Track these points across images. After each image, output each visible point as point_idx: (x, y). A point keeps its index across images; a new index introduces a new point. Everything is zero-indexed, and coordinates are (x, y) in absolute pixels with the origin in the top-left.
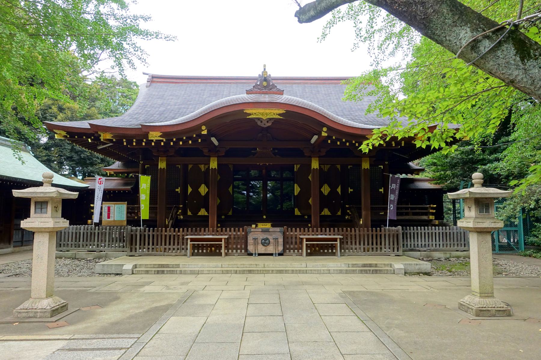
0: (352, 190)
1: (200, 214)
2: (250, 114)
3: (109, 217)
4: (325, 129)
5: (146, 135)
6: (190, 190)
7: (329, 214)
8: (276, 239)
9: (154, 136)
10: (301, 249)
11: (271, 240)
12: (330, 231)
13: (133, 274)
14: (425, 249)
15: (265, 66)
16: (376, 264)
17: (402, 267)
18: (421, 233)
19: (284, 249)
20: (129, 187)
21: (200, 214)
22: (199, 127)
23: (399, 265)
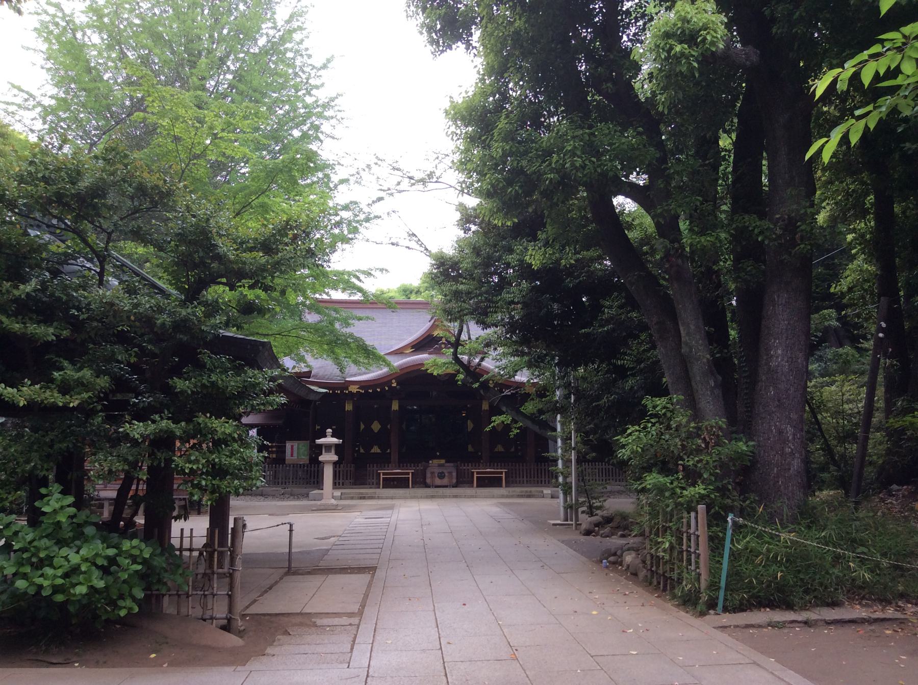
1: (372, 451)
3: (292, 455)
6: (362, 427)
7: (379, 451)
8: (450, 473)
9: (354, 389)
10: (473, 482)
20: (280, 422)
21: (372, 451)
22: (390, 382)
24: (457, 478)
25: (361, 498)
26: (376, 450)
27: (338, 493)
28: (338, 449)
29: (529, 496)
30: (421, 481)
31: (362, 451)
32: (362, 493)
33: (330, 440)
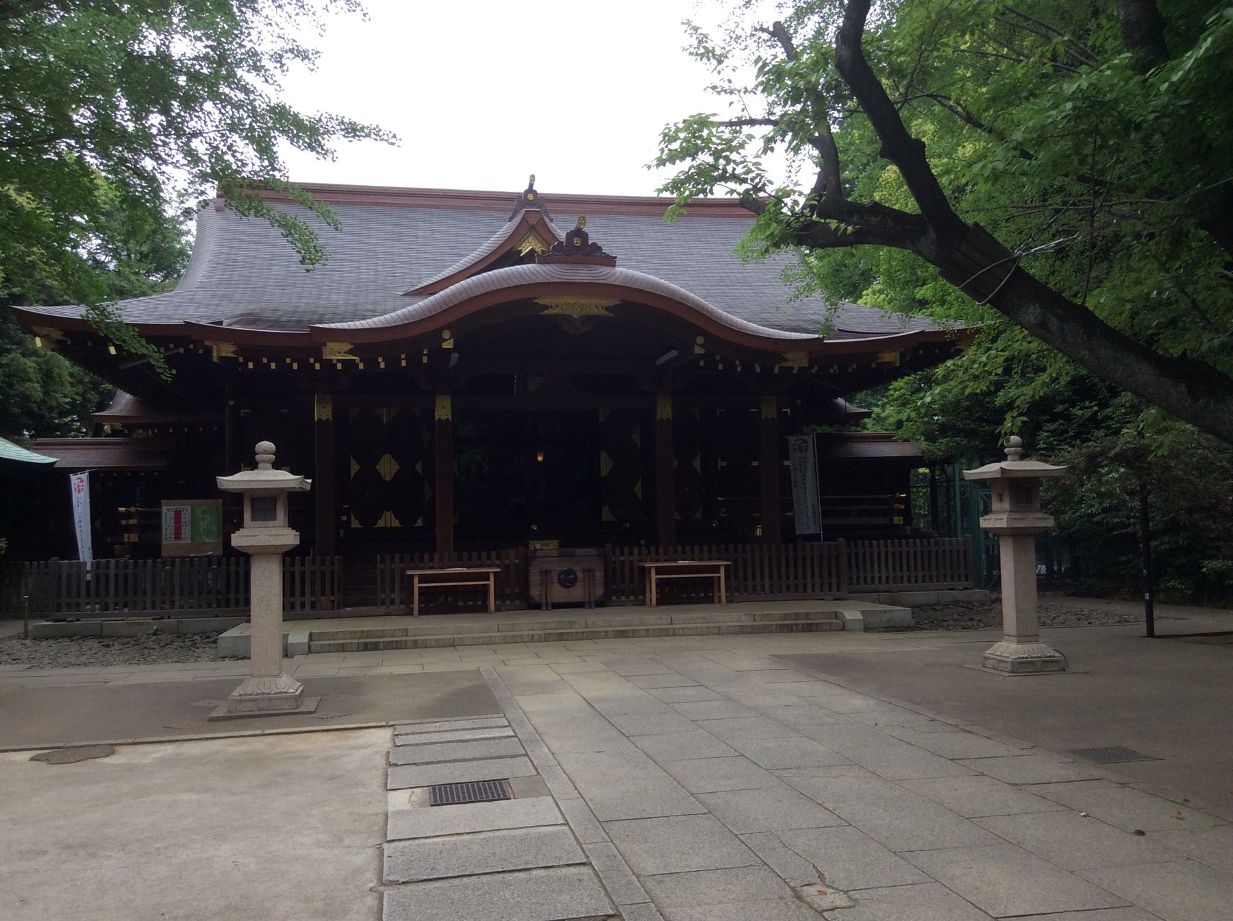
0: (724, 464)
2: (546, 307)
3: (178, 536)
4: (700, 340)
5: (317, 352)
6: (355, 467)
8: (589, 572)
9: (336, 353)
11: (580, 575)
12: (701, 552)
13: (310, 652)
14: (887, 587)
15: (533, 178)
16: (807, 614)
17: (859, 616)
18: (879, 553)
19: (606, 594)
21: (381, 524)
22: (436, 335)
23: (852, 613)
24: (606, 585)
25: (366, 647)
26: (388, 520)
27: (299, 635)
28: (298, 507)
29: (809, 628)
30: (516, 595)
31: (355, 524)
32: (369, 634)
33: (269, 476)
